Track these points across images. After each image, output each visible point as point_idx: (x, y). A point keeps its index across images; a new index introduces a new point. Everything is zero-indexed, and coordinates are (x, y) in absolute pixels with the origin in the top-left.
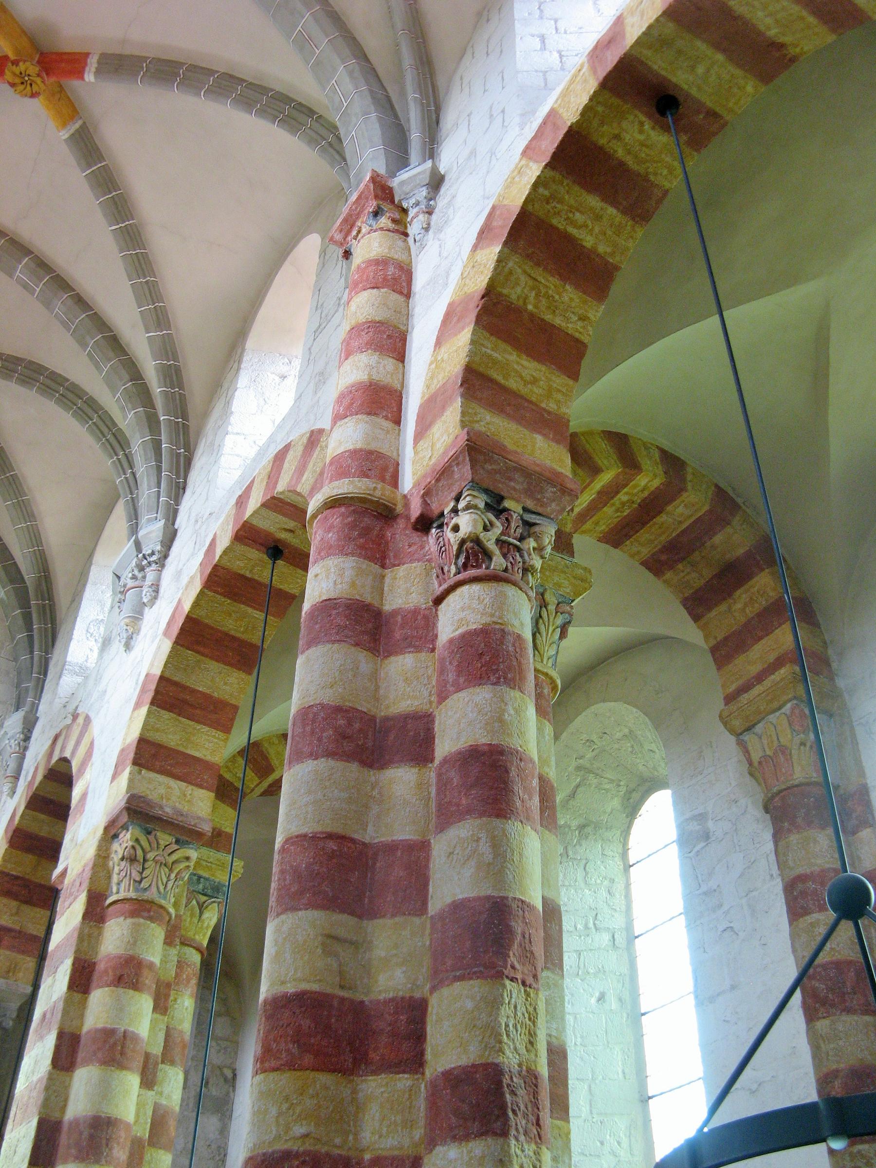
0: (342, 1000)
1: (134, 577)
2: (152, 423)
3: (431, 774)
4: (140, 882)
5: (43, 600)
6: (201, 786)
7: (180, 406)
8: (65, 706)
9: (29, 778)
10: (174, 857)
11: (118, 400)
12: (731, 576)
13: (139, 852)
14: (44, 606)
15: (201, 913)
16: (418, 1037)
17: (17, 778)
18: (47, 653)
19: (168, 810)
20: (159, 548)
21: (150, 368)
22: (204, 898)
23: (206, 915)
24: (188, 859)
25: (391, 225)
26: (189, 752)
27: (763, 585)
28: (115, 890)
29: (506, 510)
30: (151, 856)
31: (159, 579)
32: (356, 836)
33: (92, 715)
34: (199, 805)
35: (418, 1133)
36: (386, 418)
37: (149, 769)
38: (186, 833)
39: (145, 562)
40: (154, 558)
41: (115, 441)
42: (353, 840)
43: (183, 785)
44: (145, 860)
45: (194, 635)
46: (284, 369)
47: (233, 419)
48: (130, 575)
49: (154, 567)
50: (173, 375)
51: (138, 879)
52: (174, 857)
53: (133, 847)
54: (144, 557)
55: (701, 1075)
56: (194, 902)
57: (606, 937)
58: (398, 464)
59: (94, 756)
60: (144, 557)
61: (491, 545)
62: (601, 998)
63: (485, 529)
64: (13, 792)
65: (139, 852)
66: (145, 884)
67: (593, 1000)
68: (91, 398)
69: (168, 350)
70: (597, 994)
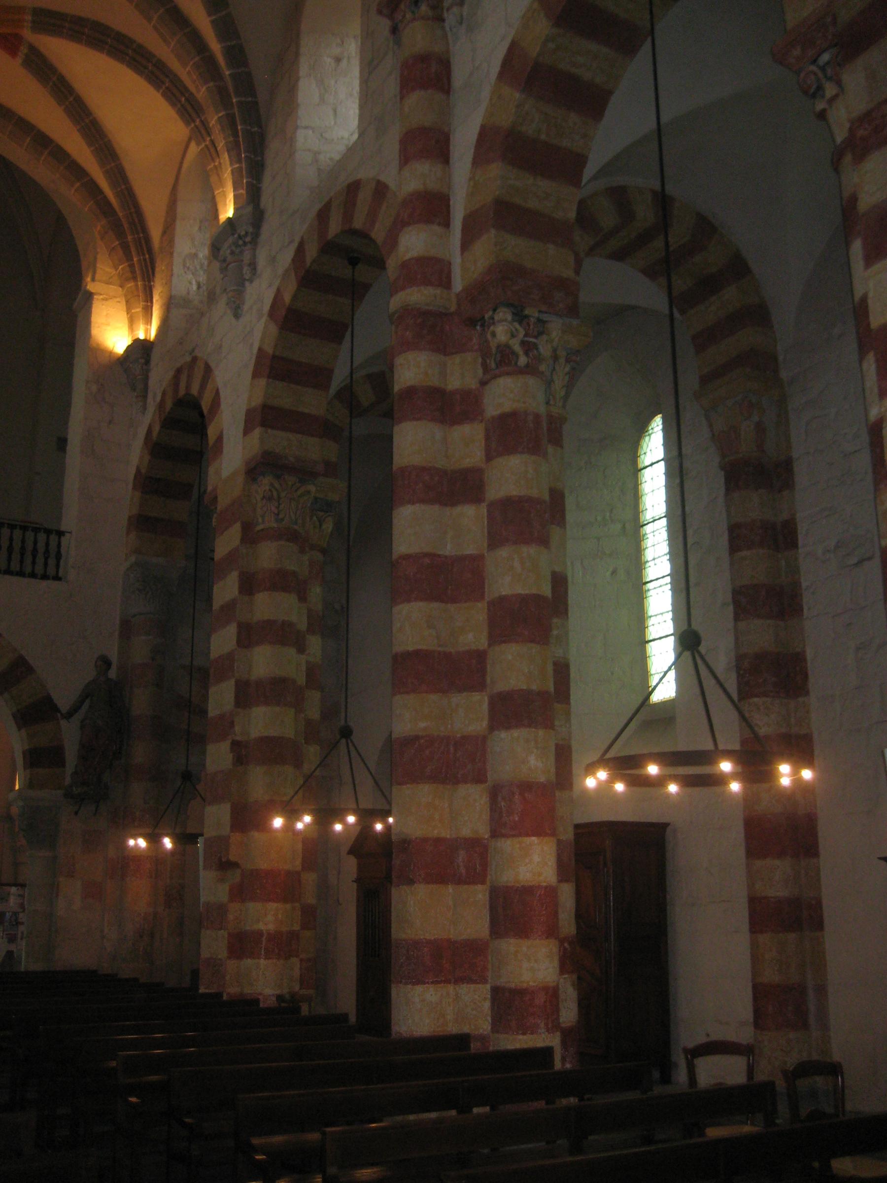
0: (439, 653)
1: (232, 253)
2: (222, 97)
3: (483, 509)
4: (278, 515)
5: (138, 233)
6: (312, 436)
7: (245, 83)
8: (181, 343)
9: (159, 398)
10: (299, 492)
11: (189, 73)
12: (709, 285)
13: (275, 493)
14: (139, 239)
15: (321, 525)
16: (483, 671)
17: (145, 397)
18: (149, 281)
19: (292, 459)
20: (251, 230)
21: (216, 47)
22: (322, 513)
23: (324, 527)
24: (309, 492)
25: (430, 13)
26: (300, 409)
27: (731, 296)
28: (260, 520)
29: (527, 317)
30: (283, 494)
31: (254, 256)
32: (439, 553)
33: (212, 365)
34: (313, 449)
35: (485, 723)
36: (439, 224)
37: (272, 428)
38: (304, 472)
39: (241, 242)
40: (248, 239)
41: (189, 109)
42: (439, 556)
43: (299, 436)
44: (279, 498)
45: (291, 320)
46: (337, 51)
47: (301, 112)
48: (229, 251)
49: (249, 246)
50: (237, 55)
51: (276, 512)
52: (299, 492)
53: (270, 490)
54: (240, 237)
55: (671, 631)
56: (315, 518)
57: (618, 526)
58: (450, 264)
59: (223, 406)
60: (240, 237)
61: (517, 348)
62: (614, 572)
63: (513, 336)
64: (145, 408)
65: (275, 493)
66: (281, 516)
67: (608, 573)
68: (159, 61)
69: (237, 55)
70: (611, 569)
